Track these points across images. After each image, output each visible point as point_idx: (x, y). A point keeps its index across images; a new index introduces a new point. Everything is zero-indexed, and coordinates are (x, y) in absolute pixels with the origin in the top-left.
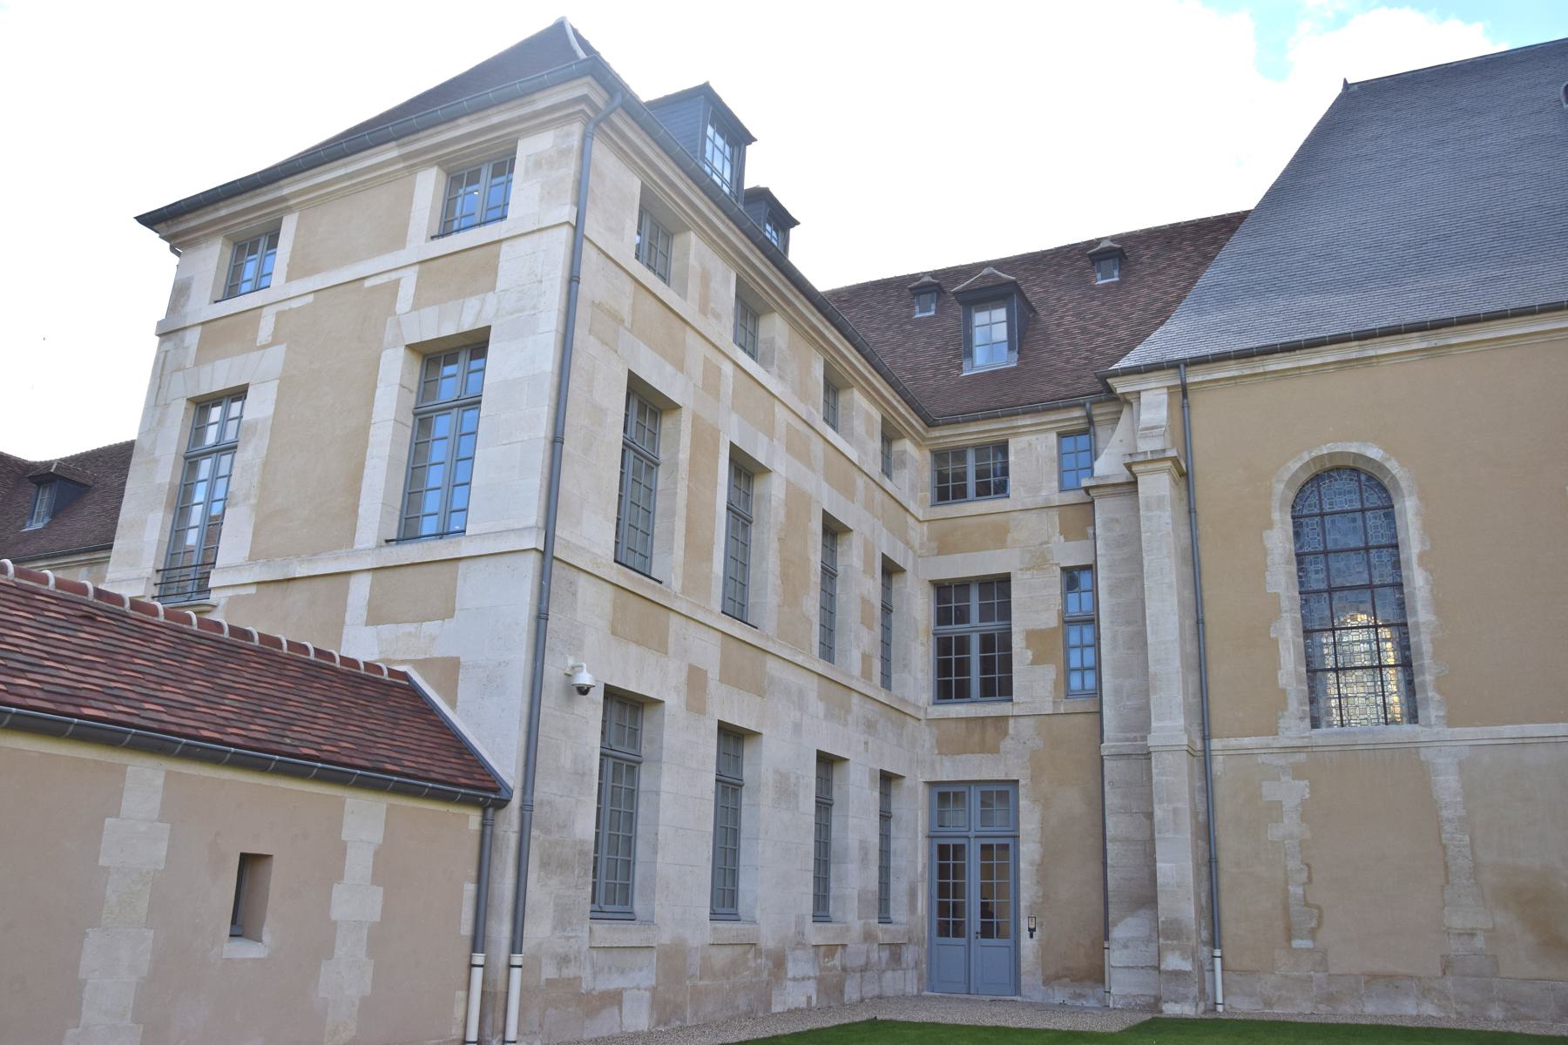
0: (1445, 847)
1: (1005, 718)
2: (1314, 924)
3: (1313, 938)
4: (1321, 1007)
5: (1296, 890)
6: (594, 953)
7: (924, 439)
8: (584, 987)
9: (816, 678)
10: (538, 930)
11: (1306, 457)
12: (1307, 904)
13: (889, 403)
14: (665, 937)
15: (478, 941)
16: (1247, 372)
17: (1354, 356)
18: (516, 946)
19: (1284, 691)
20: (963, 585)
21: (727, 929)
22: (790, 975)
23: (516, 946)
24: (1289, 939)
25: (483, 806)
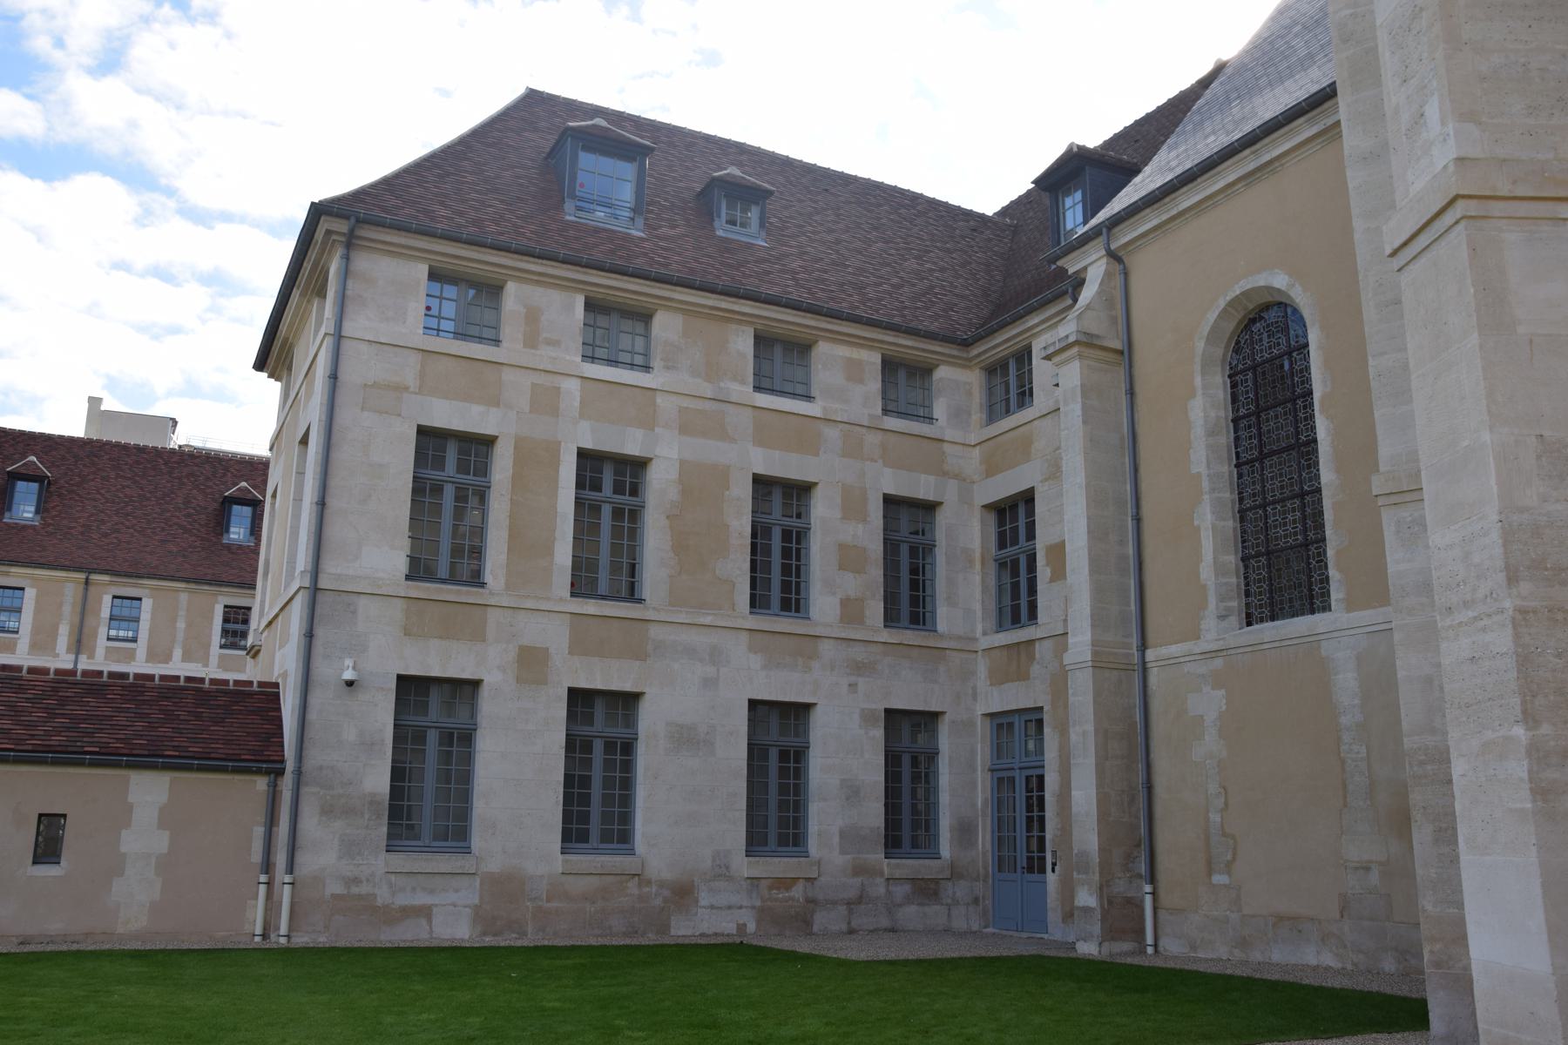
0: (1343, 762)
1: (1031, 642)
2: (1229, 857)
3: (1229, 873)
4: (1236, 952)
5: (1215, 818)
6: (393, 877)
7: (970, 360)
8: (379, 902)
9: (745, 634)
10: (308, 862)
11: (1222, 303)
12: (1224, 835)
13: (882, 342)
14: (493, 866)
15: (267, 866)
16: (1165, 217)
17: (1252, 166)
18: (290, 869)
19: (1204, 587)
20: (453, 579)
21: (778, 866)
22: (703, 903)
23: (290, 869)
24: (1210, 875)
25: (268, 772)
